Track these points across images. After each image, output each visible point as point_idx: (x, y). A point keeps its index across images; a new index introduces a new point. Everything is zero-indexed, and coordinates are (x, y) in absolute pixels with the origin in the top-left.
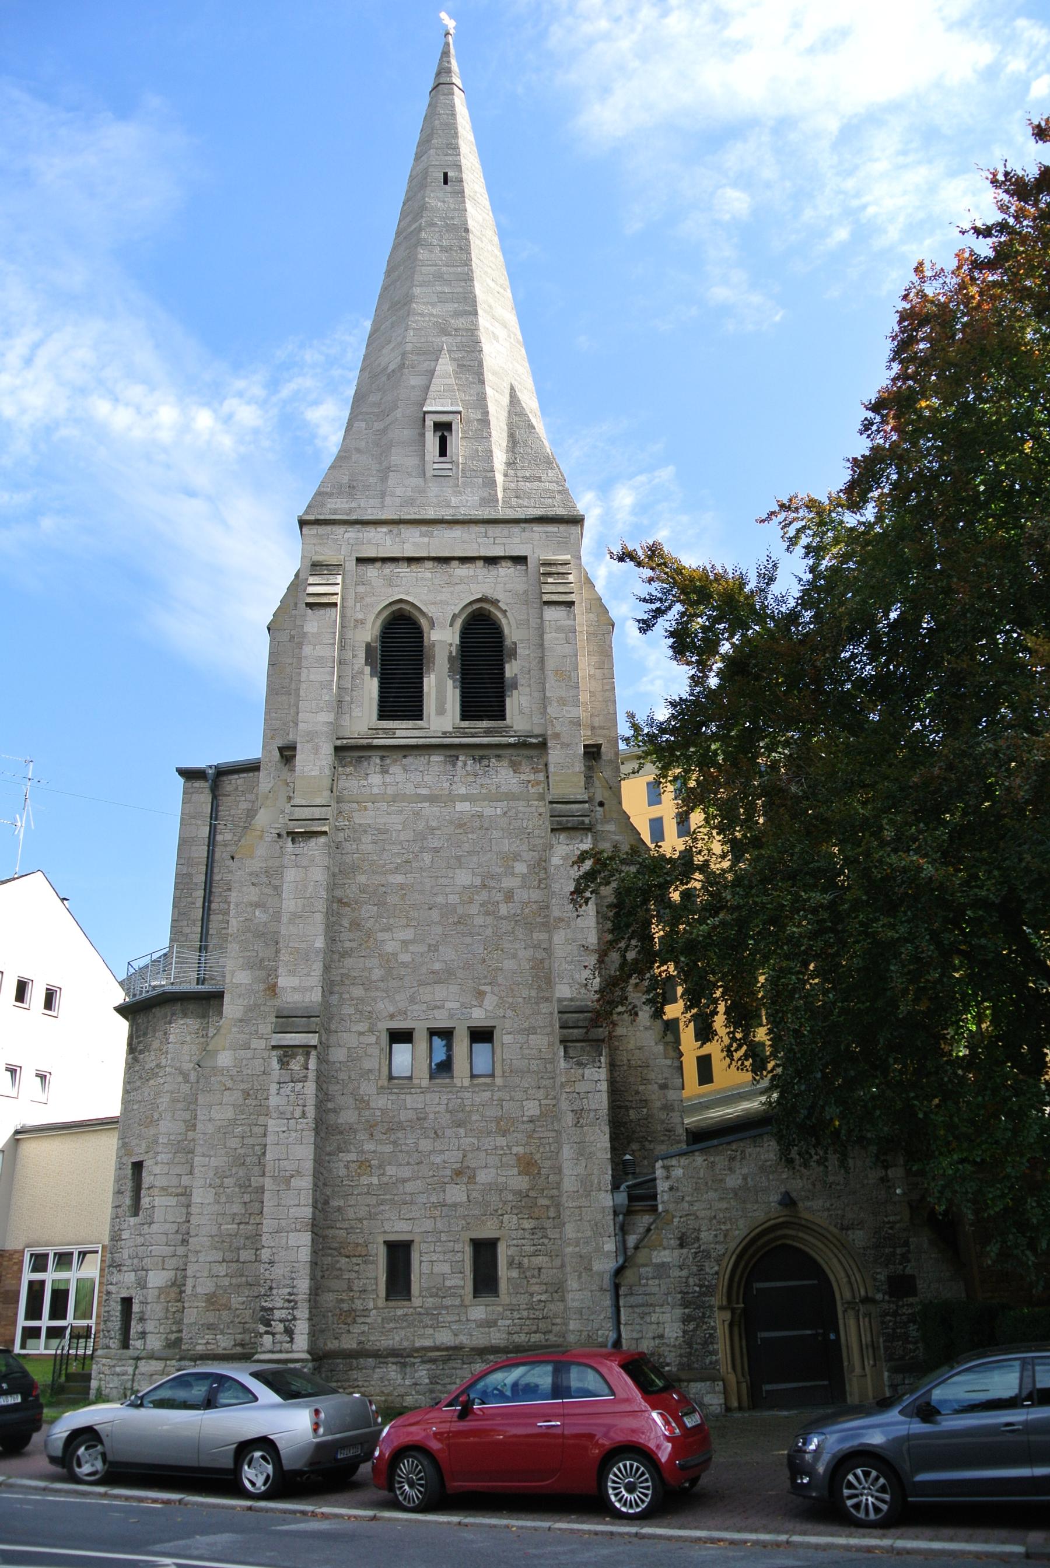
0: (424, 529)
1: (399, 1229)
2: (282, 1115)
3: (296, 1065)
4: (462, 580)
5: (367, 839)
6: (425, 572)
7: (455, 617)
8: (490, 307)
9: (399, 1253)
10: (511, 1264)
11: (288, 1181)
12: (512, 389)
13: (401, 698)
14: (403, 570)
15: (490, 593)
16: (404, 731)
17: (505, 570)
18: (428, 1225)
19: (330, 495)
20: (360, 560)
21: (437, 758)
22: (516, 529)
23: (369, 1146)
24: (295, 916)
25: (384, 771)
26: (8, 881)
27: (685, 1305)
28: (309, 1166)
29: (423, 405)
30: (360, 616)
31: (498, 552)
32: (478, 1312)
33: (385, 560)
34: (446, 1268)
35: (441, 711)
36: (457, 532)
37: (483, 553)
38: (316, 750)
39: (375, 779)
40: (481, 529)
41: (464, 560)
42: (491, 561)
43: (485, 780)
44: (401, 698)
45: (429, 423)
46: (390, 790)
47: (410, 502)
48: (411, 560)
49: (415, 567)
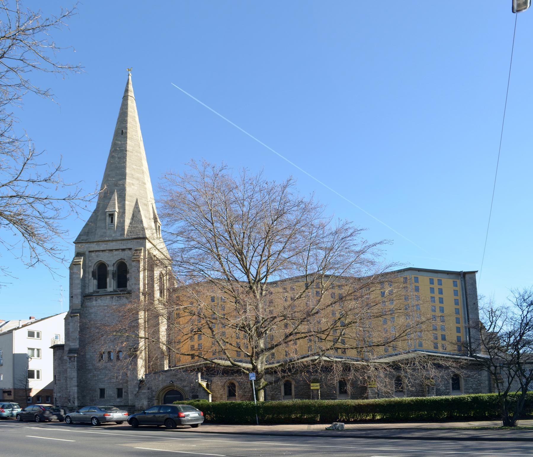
0: (105, 243)
1: (102, 386)
2: (70, 368)
3: (72, 359)
4: (116, 255)
5: (93, 315)
6: (107, 254)
7: (114, 264)
8: (133, 175)
9: (102, 391)
10: (125, 392)
11: (72, 379)
12: (137, 200)
13: (102, 284)
14: (101, 253)
15: (122, 257)
16: (101, 291)
17: (127, 252)
18: (108, 386)
19: (82, 235)
20: (90, 252)
21: (108, 297)
22: (129, 241)
23: (95, 372)
24: (72, 332)
25: (96, 300)
26: (42, 319)
27: (148, 399)
28: (76, 376)
29: (106, 208)
30: (90, 265)
31: (124, 247)
32: (118, 400)
33: (96, 251)
34: (112, 393)
35: (110, 287)
36: (114, 243)
37: (121, 248)
38: (77, 298)
39: (94, 303)
40: (120, 242)
41: (116, 250)
42: (123, 250)
43: (120, 301)
44: (102, 284)
45: (107, 214)
46: (98, 305)
47: (102, 236)
48: (103, 251)
49: (104, 253)
